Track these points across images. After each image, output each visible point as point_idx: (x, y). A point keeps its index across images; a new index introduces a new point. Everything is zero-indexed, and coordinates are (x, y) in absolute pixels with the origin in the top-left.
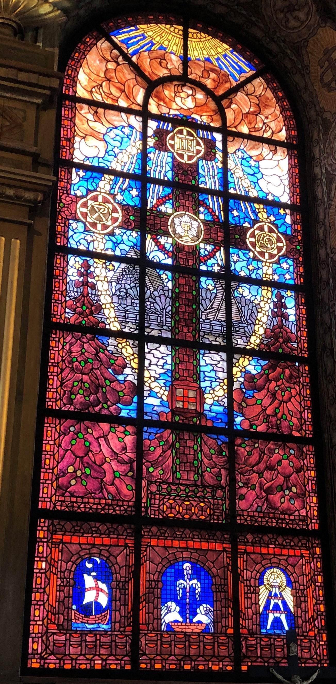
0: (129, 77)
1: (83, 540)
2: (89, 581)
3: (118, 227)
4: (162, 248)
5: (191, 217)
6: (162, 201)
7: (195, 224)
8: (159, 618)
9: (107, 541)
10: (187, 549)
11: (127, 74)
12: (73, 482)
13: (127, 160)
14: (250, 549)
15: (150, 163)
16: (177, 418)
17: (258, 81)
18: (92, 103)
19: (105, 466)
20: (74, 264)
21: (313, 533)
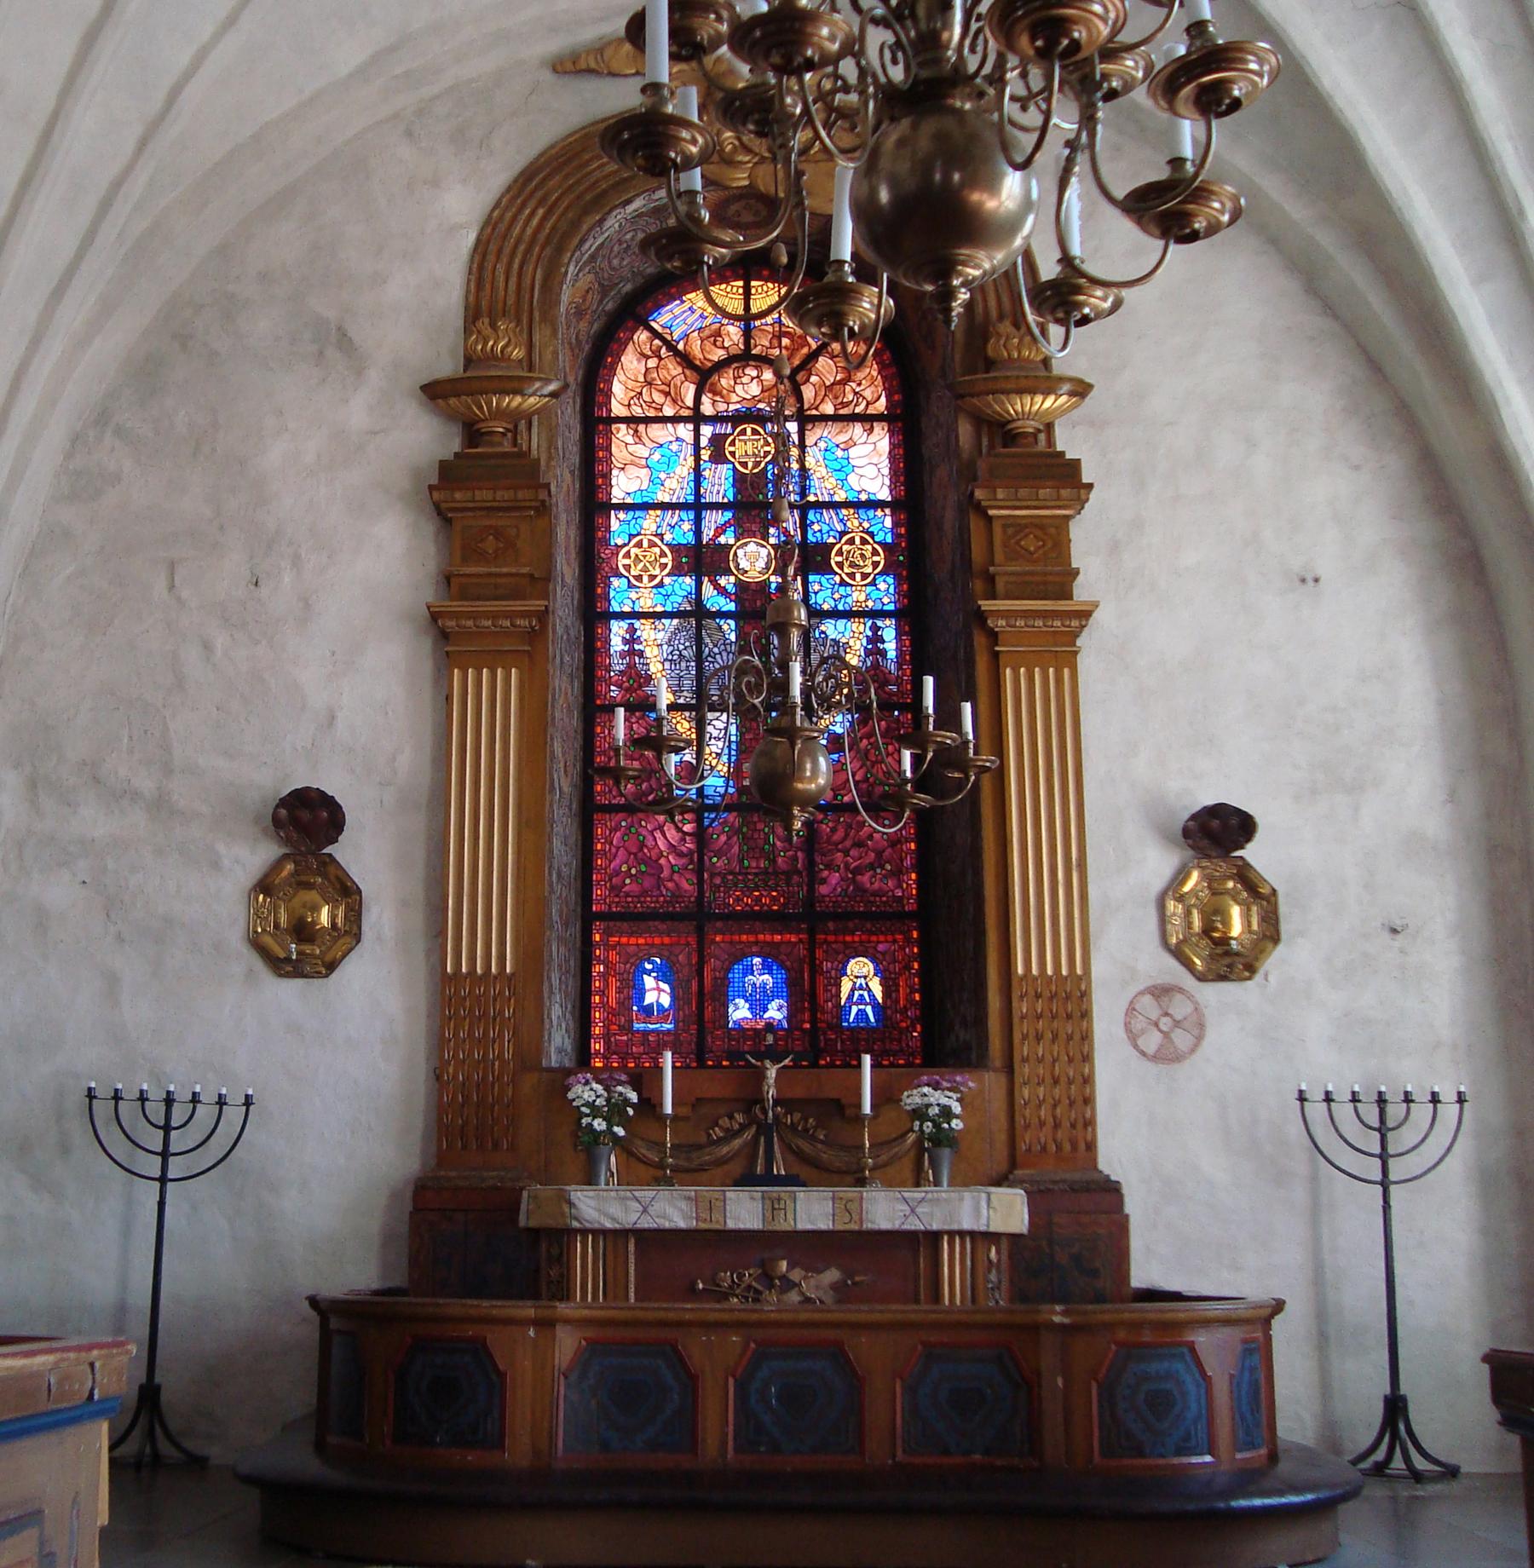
0: (674, 373)
1: (641, 941)
2: (649, 981)
3: (668, 575)
4: (722, 591)
5: (758, 544)
6: (721, 530)
7: (764, 552)
8: (726, 1016)
9: (666, 940)
10: (756, 943)
11: (674, 369)
12: (628, 881)
13: (677, 486)
14: (831, 938)
15: (705, 484)
16: (744, 799)
17: (615, 607)
18: (631, 420)
19: (662, 861)
20: (618, 629)
21: (910, 915)
